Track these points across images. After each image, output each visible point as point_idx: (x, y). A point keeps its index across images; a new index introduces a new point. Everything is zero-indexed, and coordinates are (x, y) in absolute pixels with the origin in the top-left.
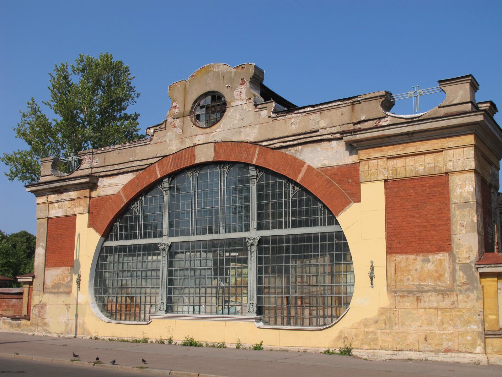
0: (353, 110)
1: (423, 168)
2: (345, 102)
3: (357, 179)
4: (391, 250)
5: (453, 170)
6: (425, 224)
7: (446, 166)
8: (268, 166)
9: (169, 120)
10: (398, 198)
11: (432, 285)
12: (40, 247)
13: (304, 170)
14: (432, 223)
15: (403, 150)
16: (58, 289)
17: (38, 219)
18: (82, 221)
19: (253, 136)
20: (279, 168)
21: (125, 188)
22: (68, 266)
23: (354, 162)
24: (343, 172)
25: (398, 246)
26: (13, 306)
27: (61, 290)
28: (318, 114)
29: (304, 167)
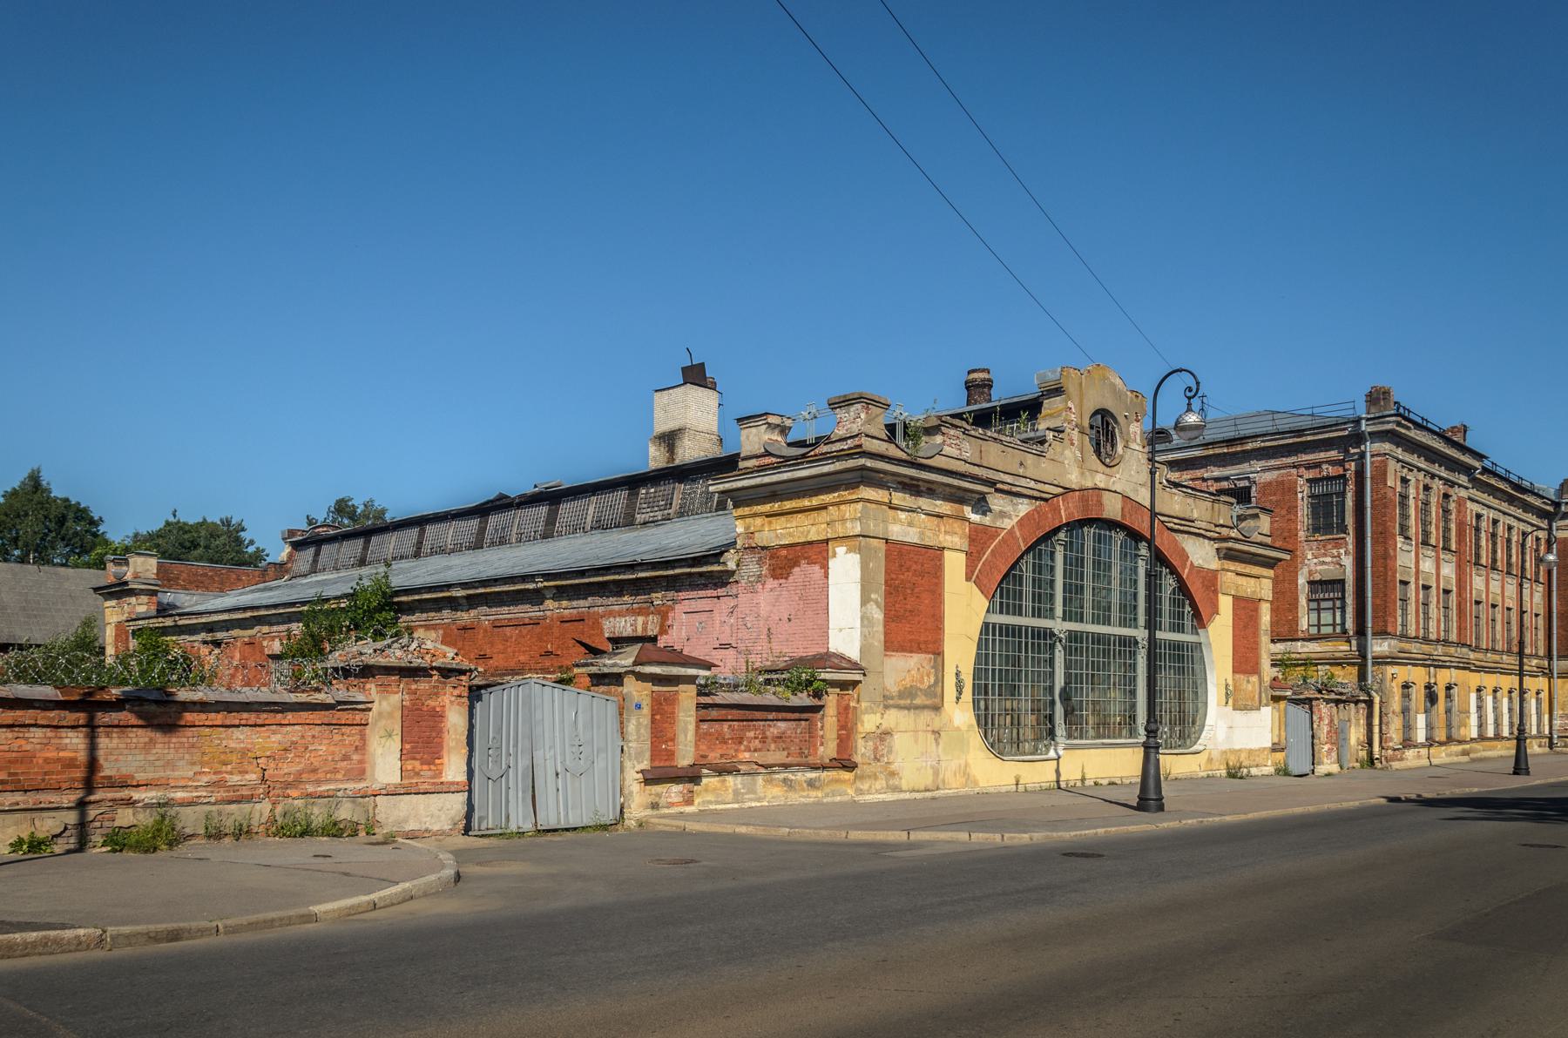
4: (1234, 672)
12: (872, 603)
15: (1245, 568)
16: (912, 700)
18: (954, 564)
22: (929, 653)
26: (779, 738)
27: (918, 701)
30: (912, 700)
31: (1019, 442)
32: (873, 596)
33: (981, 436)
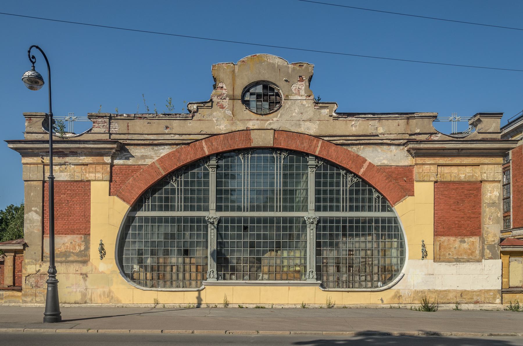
0: (408, 123)
1: (464, 175)
2: (402, 116)
3: (411, 178)
4: (437, 233)
5: (486, 180)
6: (462, 216)
7: (482, 176)
8: (331, 158)
9: (215, 99)
10: (443, 196)
11: (466, 259)
13: (365, 166)
14: (468, 216)
16: (66, 258)
17: (25, 181)
19: (313, 130)
20: (341, 161)
21: (161, 160)
23: (409, 165)
24: (399, 172)
25: (442, 230)
27: (71, 259)
28: (377, 121)
29: (366, 164)
30: (66, 258)
31: (161, 116)
32: (33, 209)
33: (127, 118)
